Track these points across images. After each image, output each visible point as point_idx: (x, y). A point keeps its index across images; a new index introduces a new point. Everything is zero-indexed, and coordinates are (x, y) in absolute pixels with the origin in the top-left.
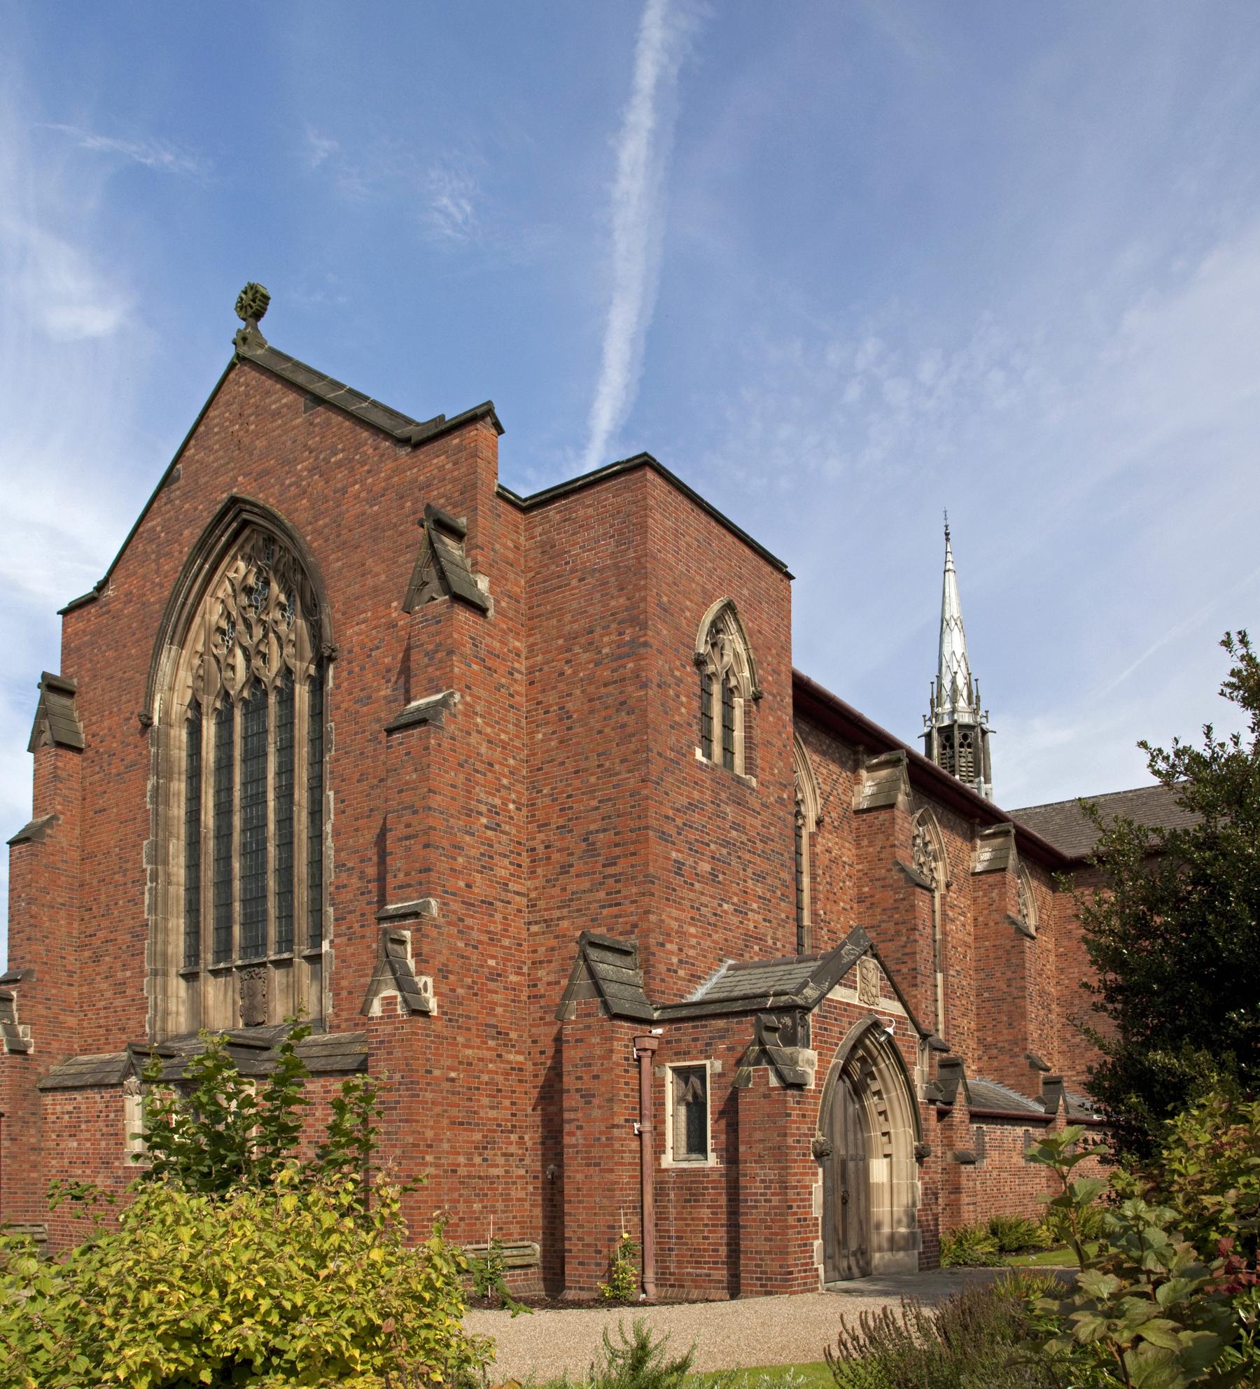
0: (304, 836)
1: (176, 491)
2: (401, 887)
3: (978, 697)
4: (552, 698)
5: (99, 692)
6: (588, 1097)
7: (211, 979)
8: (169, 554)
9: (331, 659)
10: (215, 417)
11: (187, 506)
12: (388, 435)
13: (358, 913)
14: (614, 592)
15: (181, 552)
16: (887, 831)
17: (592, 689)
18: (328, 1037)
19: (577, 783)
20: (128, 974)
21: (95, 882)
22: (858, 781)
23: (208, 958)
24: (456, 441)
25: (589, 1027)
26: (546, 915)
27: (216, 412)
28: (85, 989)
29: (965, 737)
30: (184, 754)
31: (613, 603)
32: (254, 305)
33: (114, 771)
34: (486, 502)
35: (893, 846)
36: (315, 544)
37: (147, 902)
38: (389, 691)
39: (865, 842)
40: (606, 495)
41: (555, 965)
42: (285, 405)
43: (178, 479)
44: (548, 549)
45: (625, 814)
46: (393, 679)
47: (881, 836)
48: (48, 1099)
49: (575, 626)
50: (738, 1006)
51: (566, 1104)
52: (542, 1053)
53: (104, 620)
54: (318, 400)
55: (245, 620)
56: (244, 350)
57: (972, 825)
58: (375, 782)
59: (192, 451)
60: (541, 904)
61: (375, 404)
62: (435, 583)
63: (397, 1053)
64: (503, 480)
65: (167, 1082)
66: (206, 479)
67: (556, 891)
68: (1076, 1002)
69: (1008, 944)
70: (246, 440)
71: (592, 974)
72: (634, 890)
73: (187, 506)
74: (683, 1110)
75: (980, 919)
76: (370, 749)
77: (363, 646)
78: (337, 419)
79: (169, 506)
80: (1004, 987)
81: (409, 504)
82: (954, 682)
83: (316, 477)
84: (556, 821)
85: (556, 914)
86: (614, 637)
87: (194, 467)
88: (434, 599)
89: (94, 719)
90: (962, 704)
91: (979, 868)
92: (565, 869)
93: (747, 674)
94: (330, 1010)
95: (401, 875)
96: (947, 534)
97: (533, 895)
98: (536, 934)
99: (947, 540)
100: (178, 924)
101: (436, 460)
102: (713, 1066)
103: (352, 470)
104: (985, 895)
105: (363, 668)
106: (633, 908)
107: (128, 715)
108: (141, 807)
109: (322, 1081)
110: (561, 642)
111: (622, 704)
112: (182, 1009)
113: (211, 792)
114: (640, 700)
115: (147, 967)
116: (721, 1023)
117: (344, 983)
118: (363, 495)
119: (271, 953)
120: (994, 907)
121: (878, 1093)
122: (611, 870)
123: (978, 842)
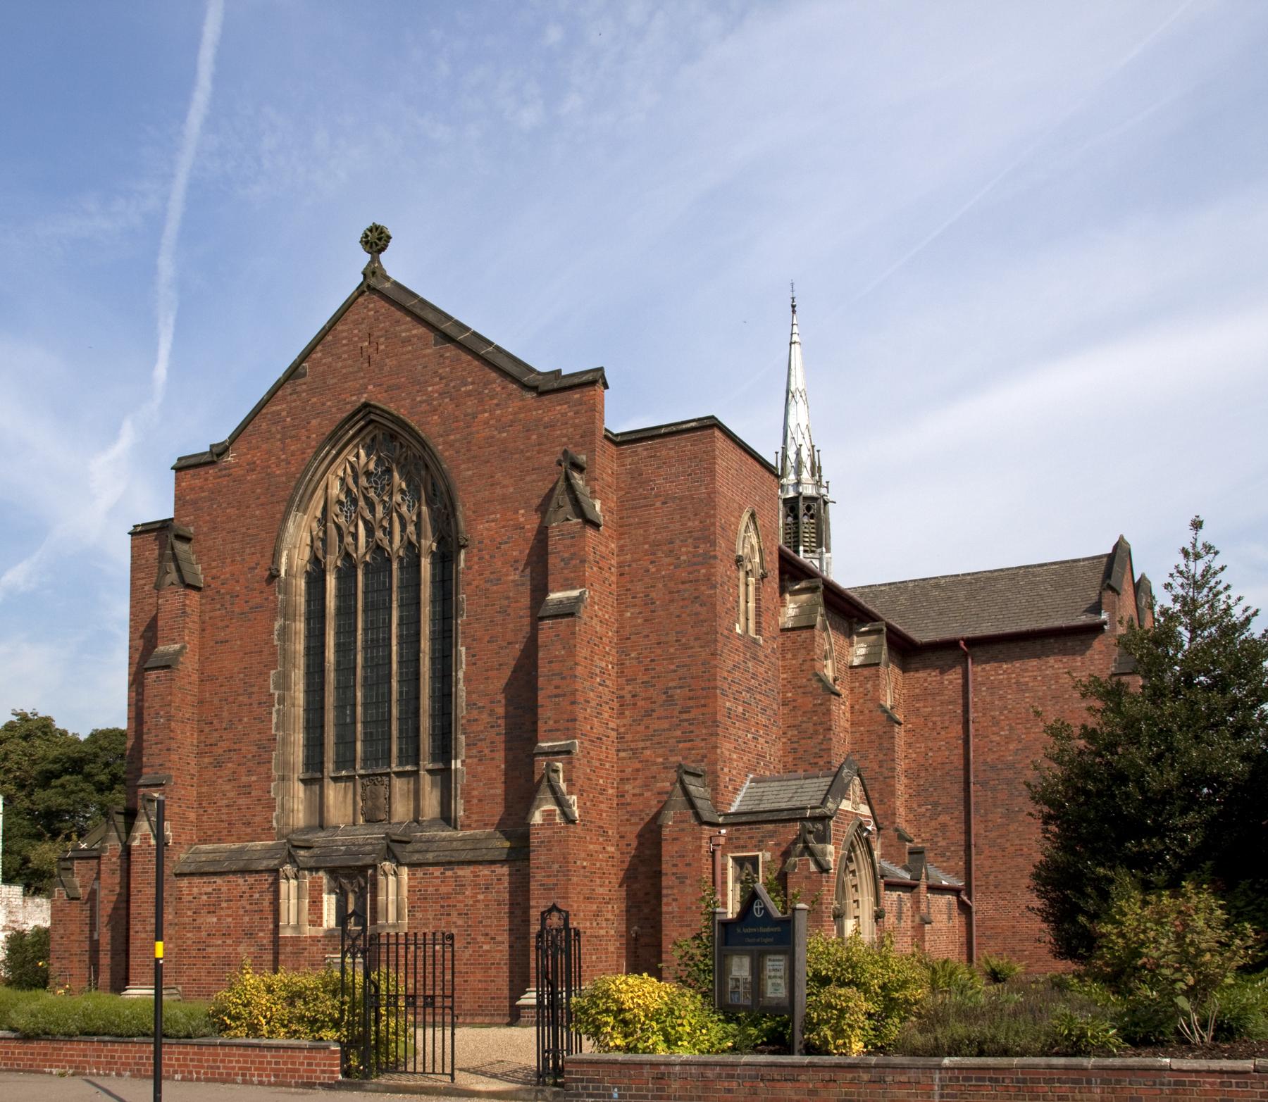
0: (427, 677)
1: (302, 385)
2: (550, 731)
3: (820, 468)
4: (639, 587)
5: (219, 542)
6: (681, 879)
7: (332, 783)
8: (296, 438)
9: (464, 547)
10: (343, 331)
11: (314, 400)
12: (515, 380)
13: (488, 741)
14: (691, 515)
15: (308, 437)
16: (809, 646)
17: (671, 584)
18: (461, 834)
19: (659, 651)
20: (254, 778)
21: (216, 701)
22: (783, 604)
23: (329, 767)
24: (577, 396)
25: (683, 830)
26: (633, 745)
27: (344, 327)
28: (204, 789)
29: (809, 508)
30: (303, 600)
31: (690, 524)
32: (376, 240)
33: (237, 610)
34: (600, 442)
35: (813, 660)
36: (447, 454)
37: (274, 721)
38: (517, 577)
39: (789, 656)
40: (684, 442)
41: (638, 782)
42: (415, 336)
43: (304, 375)
44: (635, 474)
45: (697, 677)
46: (521, 568)
47: (803, 651)
48: (184, 882)
49: (659, 537)
50: (784, 816)
51: (664, 883)
52: (628, 845)
53: (224, 481)
54: (447, 338)
55: (366, 499)
56: (372, 281)
57: (851, 624)
58: (505, 644)
59: (319, 355)
60: (629, 737)
61: (498, 348)
62: (568, 508)
63: (556, 850)
64: (607, 425)
65: (317, 869)
66: (335, 381)
67: (641, 728)
68: (923, 774)
69: (881, 730)
70: (375, 357)
71: (686, 792)
72: (704, 731)
73: (314, 400)
74: (738, 886)
75: (857, 707)
76: (499, 618)
77: (493, 540)
78: (466, 358)
79: (295, 396)
80: (876, 767)
81: (534, 437)
82: (798, 453)
83: (447, 400)
84: (641, 677)
85: (641, 745)
86: (690, 549)
87: (321, 369)
88: (568, 520)
89: (214, 564)
90: (806, 475)
91: (856, 662)
92: (648, 713)
93: (757, 560)
94: (462, 813)
95: (551, 722)
96: (793, 307)
97: (622, 730)
98: (624, 759)
99: (794, 312)
100: (299, 738)
101: (557, 408)
102: (764, 856)
103: (481, 401)
104: (861, 686)
105: (492, 557)
106: (703, 744)
107: (253, 565)
108: (269, 642)
109: (471, 868)
110: (646, 547)
111: (696, 598)
112: (301, 807)
113: (332, 633)
114: (710, 596)
115: (274, 773)
116: (770, 827)
117: (475, 793)
118: (492, 422)
119: (393, 765)
120: (868, 697)
121: (853, 872)
122: (685, 716)
123: (855, 638)
